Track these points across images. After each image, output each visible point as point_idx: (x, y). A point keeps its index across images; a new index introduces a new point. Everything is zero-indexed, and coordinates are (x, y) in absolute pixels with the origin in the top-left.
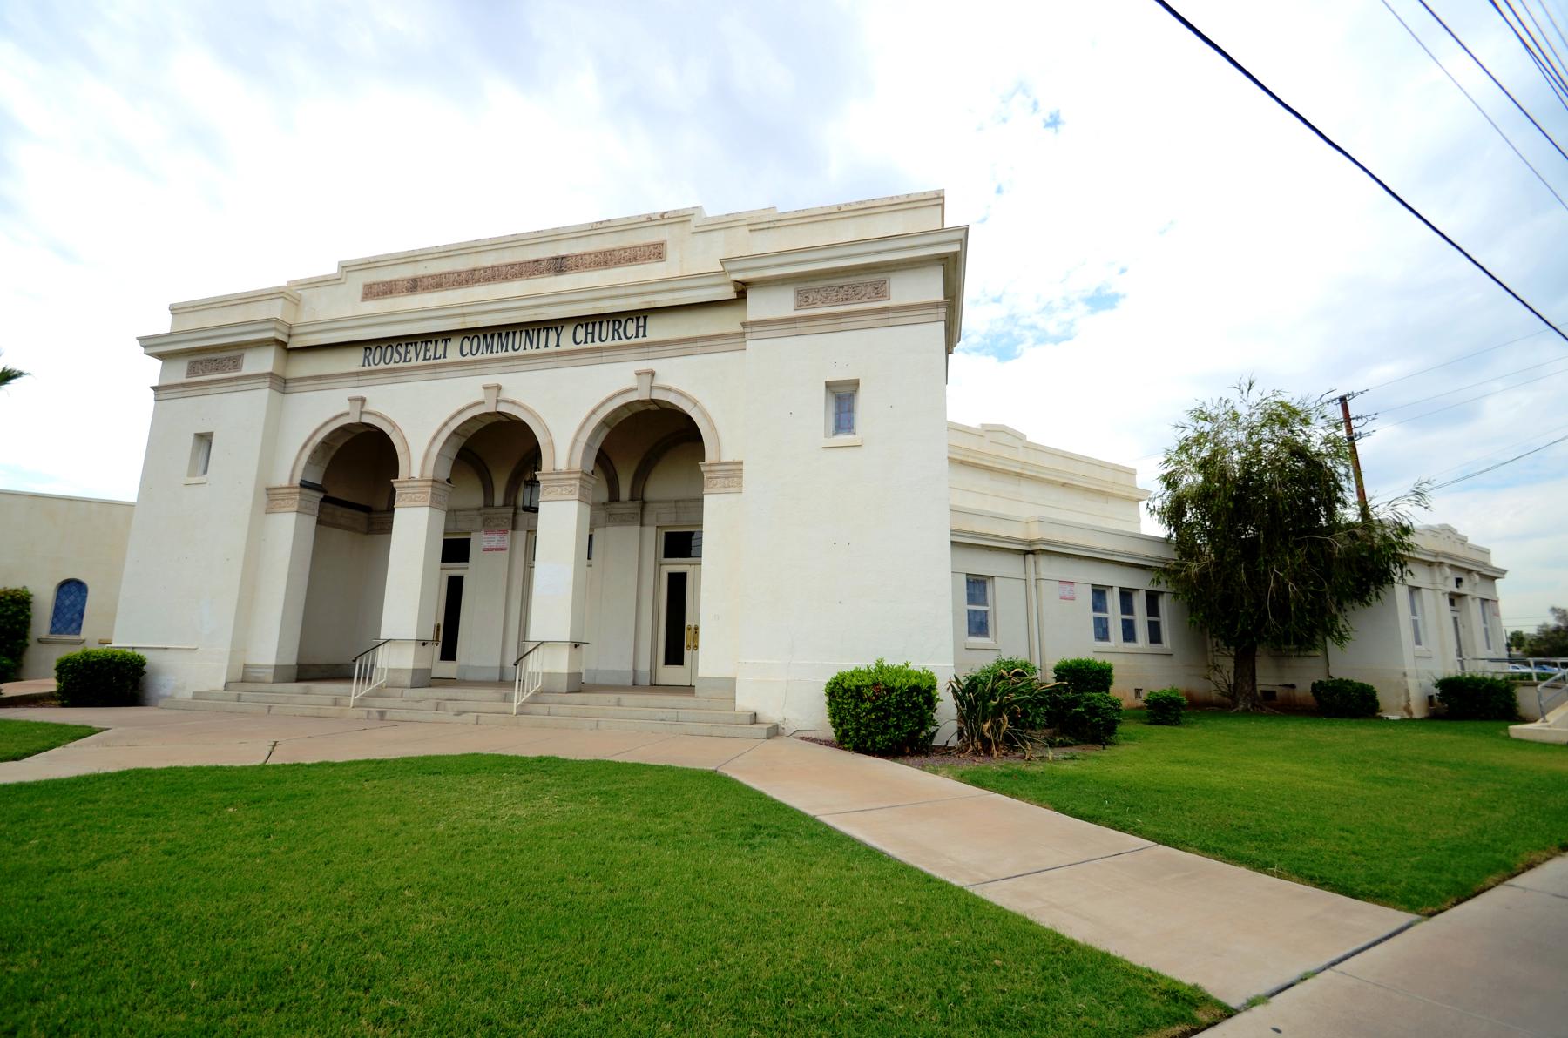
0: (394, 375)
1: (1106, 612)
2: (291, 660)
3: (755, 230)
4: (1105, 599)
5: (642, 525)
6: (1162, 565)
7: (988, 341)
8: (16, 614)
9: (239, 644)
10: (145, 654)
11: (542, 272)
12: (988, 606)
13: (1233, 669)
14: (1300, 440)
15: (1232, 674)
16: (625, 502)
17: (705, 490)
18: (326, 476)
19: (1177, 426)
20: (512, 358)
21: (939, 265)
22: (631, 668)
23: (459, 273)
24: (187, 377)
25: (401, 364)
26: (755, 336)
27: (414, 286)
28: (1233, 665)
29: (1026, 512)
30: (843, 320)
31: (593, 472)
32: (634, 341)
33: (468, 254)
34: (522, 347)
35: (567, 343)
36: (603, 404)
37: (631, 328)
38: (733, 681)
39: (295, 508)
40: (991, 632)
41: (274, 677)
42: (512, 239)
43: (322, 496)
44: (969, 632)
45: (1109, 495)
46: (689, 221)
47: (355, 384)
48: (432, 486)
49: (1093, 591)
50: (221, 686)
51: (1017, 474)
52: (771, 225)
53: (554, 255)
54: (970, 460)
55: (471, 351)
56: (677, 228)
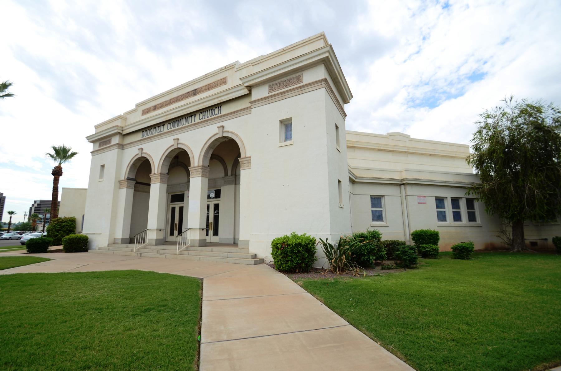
0: (150, 139)
1: (444, 208)
2: (127, 236)
3: (254, 65)
4: (444, 203)
5: (235, 184)
6: (469, 186)
7: (424, 101)
8: (71, 225)
9: (112, 231)
10: (88, 236)
11: (190, 96)
12: (382, 208)
13: (512, 232)
14: (540, 122)
15: (511, 235)
16: (229, 176)
17: (241, 168)
18: (137, 175)
19: (477, 123)
20: (181, 128)
21: (322, 64)
22: (233, 237)
23: (167, 101)
24: (99, 148)
25: (152, 135)
26: (254, 106)
27: (155, 108)
28: (512, 230)
29: (399, 167)
30: (285, 94)
31: (208, 166)
32: (217, 115)
33: (169, 94)
34: (184, 124)
35: (197, 120)
36: (208, 140)
37: (217, 110)
38: (249, 241)
39: (126, 187)
40: (384, 219)
41: (121, 242)
42: (181, 86)
43: (135, 182)
44: (438, 220)
45: (455, 158)
46: (234, 67)
47: (140, 144)
48: (160, 176)
49: (436, 199)
50: (106, 245)
51: (406, 152)
52: (259, 62)
53: (193, 89)
54: (382, 148)
55: (170, 128)
56: (230, 71)
